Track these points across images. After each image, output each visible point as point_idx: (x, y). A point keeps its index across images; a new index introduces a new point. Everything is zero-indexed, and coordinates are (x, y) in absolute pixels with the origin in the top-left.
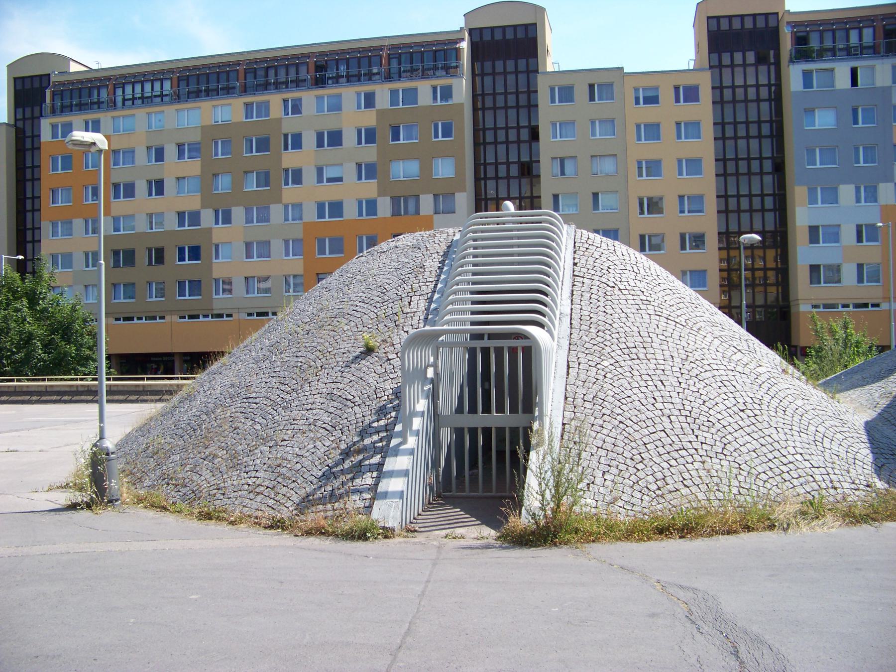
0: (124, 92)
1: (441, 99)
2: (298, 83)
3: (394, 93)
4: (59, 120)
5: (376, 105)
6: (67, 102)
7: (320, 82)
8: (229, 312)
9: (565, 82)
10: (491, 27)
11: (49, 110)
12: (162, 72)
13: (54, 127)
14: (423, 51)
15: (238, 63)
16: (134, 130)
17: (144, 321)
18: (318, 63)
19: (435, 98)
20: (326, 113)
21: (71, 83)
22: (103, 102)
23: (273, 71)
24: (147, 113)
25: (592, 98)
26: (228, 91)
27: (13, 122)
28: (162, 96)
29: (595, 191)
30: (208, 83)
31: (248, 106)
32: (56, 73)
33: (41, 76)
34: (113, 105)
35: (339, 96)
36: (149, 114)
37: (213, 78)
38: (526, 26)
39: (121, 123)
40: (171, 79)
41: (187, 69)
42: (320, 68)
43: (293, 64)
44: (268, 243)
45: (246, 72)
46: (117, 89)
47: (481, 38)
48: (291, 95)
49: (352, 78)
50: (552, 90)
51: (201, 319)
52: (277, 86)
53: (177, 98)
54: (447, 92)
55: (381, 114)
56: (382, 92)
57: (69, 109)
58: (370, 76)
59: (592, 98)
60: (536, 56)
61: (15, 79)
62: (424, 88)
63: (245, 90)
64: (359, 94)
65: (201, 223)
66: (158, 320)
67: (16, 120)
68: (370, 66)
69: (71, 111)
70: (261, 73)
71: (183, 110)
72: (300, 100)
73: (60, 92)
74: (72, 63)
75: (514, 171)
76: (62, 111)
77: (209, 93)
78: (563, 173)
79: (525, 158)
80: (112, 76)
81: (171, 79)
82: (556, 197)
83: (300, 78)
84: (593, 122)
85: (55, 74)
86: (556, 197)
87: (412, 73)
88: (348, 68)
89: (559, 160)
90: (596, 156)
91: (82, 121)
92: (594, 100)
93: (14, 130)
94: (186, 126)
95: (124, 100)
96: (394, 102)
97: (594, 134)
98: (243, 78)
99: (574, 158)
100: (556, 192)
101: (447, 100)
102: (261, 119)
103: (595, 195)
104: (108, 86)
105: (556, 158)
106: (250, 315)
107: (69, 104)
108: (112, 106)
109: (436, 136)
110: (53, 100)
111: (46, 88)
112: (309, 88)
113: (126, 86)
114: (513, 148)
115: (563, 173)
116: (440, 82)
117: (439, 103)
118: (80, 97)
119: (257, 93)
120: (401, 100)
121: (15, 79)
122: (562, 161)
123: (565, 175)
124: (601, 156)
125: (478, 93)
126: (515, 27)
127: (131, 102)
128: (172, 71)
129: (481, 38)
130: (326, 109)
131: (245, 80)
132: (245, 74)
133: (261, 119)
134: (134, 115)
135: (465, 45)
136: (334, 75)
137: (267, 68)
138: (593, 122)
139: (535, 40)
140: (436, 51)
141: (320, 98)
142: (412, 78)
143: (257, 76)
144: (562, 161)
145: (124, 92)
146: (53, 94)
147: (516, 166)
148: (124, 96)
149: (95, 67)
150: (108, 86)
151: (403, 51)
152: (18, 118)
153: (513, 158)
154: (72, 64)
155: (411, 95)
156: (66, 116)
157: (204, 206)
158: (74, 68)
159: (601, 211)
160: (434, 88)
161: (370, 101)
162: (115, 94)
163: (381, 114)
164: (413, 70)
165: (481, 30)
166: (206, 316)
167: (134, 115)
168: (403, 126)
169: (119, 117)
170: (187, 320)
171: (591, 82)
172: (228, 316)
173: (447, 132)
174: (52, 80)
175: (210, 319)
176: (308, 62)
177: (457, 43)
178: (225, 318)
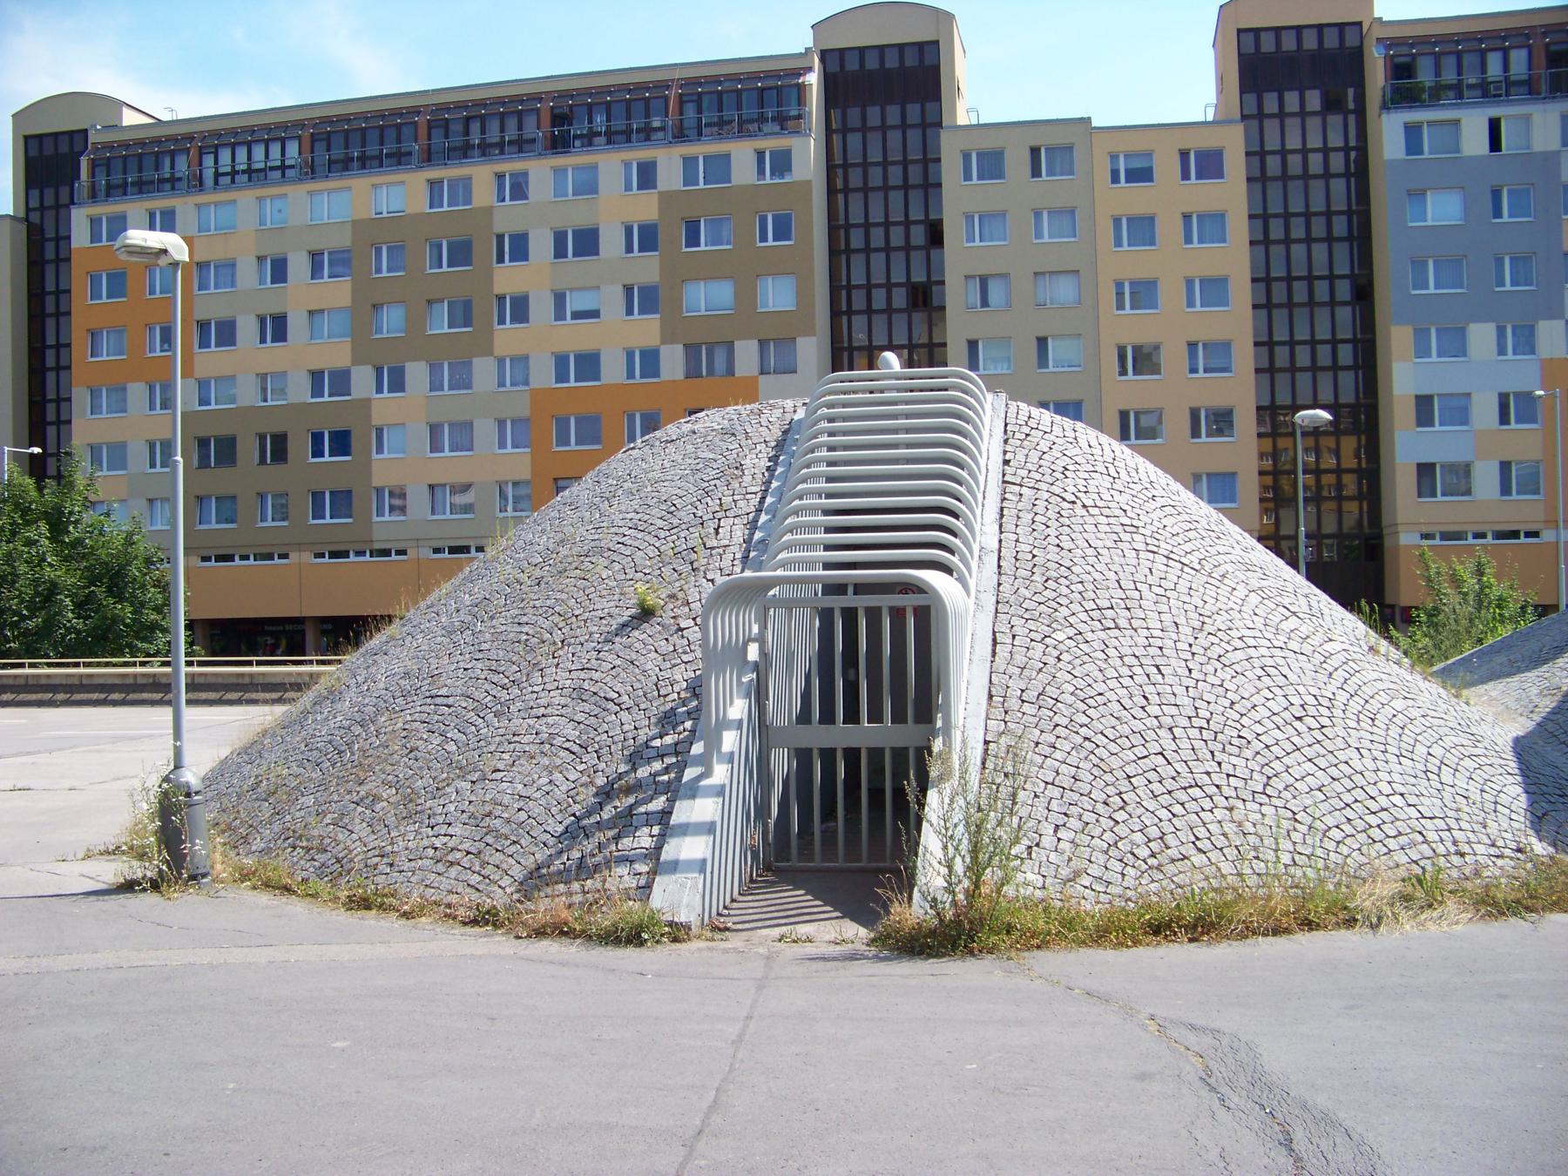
0: (216, 162)
1: (772, 174)
2: (521, 145)
3: (689, 162)
4: (104, 210)
5: (659, 184)
6: (117, 178)
7: (559, 144)
8: (401, 546)
9: (989, 143)
10: (859, 48)
11: (85, 193)
12: (284, 126)
13: (95, 222)
14: (741, 90)
15: (416, 111)
16: (234, 228)
17: (252, 561)
18: (557, 111)
19: (761, 172)
20: (570, 197)
21: (125, 145)
22: (180, 179)
23: (478, 124)
24: (257, 198)
25: (1036, 172)
26: (400, 159)
27: (22, 214)
28: (283, 168)
29: (1041, 334)
30: (364, 146)
31: (434, 185)
32: (99, 127)
33: (71, 134)
34: (198, 184)
35: (594, 168)
36: (260, 199)
37: (373, 136)
38: (920, 46)
39: (213, 215)
40: (299, 138)
41: (327, 120)
42: (560, 119)
43: (512, 112)
44: (469, 425)
45: (430, 126)
46: (204, 156)
47: (842, 66)
48: (510, 166)
49: (617, 137)
50: (967, 157)
51: (352, 558)
52: (485, 150)
53: (310, 171)
54: (782, 162)
55: (667, 199)
56: (669, 161)
57: (120, 190)
58: (647, 134)
59: (1036, 172)
60: (937, 97)
61: (27, 138)
62: (742, 154)
63: (428, 158)
64: (627, 165)
65: (352, 391)
66: (277, 561)
67: (28, 210)
68: (647, 115)
69: (125, 194)
70: (457, 128)
71: (320, 192)
72: (525, 174)
73: (104, 162)
74: (125, 111)
75: (900, 298)
76: (108, 195)
77: (366, 163)
78: (985, 303)
79: (919, 277)
80: (195, 133)
81: (299, 138)
82: (973, 345)
83: (525, 137)
84: (1038, 214)
85: (96, 130)
86: (973, 345)
87: (722, 128)
88: (608, 120)
89: (978, 279)
90: (1043, 273)
91: (144, 211)
92: (1040, 175)
93: (24, 227)
94: (326, 221)
95: (217, 175)
96: (689, 178)
97: (1039, 235)
98: (426, 137)
99: (1004, 276)
100: (973, 337)
101: (782, 176)
102: (456, 208)
103: (1042, 342)
104: (188, 150)
105: (973, 277)
106: (437, 551)
107: (120, 181)
108: (195, 186)
109: (764, 238)
110: (93, 174)
111: (81, 154)
112: (540, 154)
113: (220, 150)
114: (898, 259)
115: (985, 303)
116: (770, 144)
117: (768, 180)
118: (140, 170)
119: (449, 162)
120: (701, 175)
121: (27, 138)
122: (984, 281)
123: (988, 306)
124: (1051, 273)
125: (837, 162)
126: (901, 47)
127: (228, 178)
128: (300, 124)
129: (842, 66)
130: (570, 191)
131: (429, 139)
132: (430, 129)
133: (456, 208)
134: (234, 202)
135: (813, 79)
136: (585, 132)
137: (468, 120)
138: (1038, 214)
139: (936, 70)
140: (762, 90)
141: (559, 172)
142: (720, 137)
143: (450, 133)
144: (984, 281)
145: (216, 162)
146: (94, 165)
147: (903, 290)
148: (217, 169)
149: (166, 117)
150: (188, 150)
151: (705, 90)
152: (31, 206)
153: (898, 276)
154: (126, 112)
155: (719, 167)
156: (116, 202)
157: (357, 361)
158: (129, 119)
159: (1051, 369)
160: (760, 154)
161: (647, 177)
162: (201, 165)
163: (667, 199)
164: (722, 123)
165: (842, 52)
166: (360, 553)
167: (234, 202)
168: (705, 220)
169: (208, 204)
170: (326, 560)
171: (1034, 143)
172: (399, 553)
173: (782, 232)
174: (90, 141)
175: (368, 557)
176: (539, 108)
177: (800, 75)
178: (394, 557)
